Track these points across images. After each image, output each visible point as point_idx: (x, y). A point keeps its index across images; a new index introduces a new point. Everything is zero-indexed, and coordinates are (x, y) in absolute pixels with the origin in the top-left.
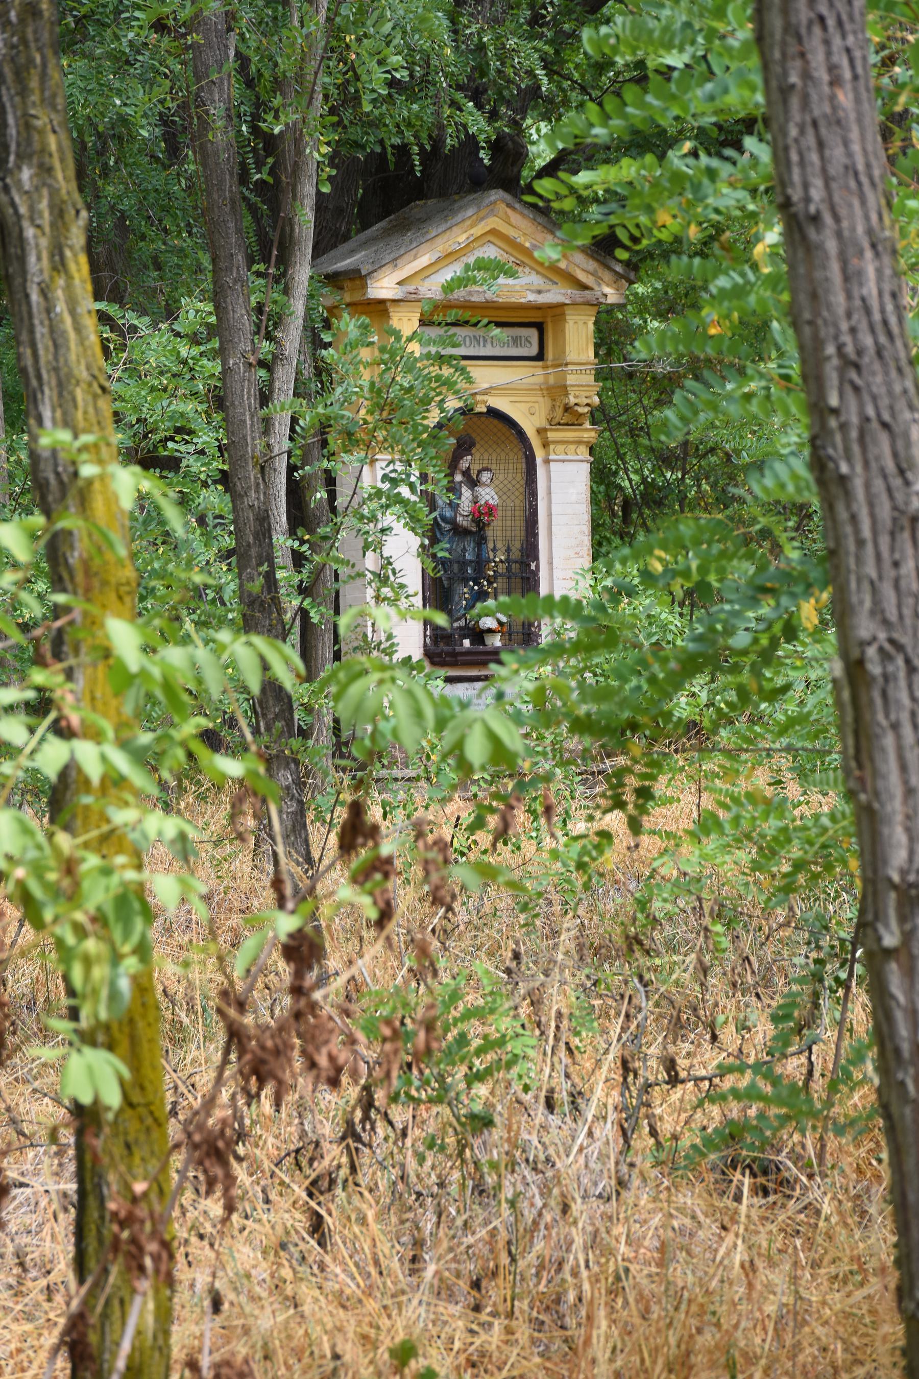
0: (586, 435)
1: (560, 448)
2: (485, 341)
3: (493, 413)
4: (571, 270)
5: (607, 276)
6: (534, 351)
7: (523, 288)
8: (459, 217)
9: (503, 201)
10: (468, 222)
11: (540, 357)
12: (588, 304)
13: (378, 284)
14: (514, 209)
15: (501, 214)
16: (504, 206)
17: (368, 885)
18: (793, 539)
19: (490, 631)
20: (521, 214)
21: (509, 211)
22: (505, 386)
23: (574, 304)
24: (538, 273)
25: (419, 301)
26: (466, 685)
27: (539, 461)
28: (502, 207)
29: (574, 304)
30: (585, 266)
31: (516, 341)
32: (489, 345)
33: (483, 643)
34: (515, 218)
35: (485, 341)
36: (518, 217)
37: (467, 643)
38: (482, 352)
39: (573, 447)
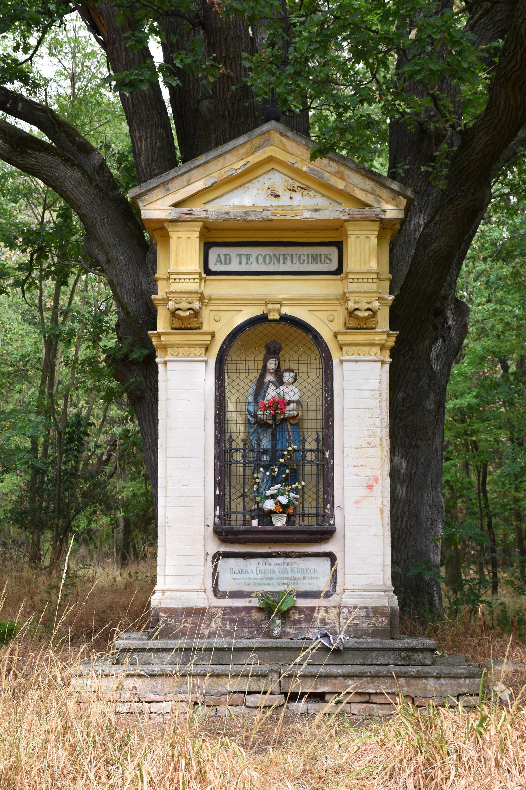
0: (377, 337)
1: (350, 350)
2: (285, 259)
3: (285, 319)
4: (349, 190)
5: (385, 194)
6: (334, 266)
7: (304, 206)
8: (230, 145)
9: (276, 130)
10: (243, 151)
11: (339, 271)
12: (366, 219)
13: (151, 206)
14: (287, 137)
15: (277, 143)
16: (278, 135)
17: (417, 633)
18: (137, 515)
19: (272, 512)
20: (294, 141)
21: (283, 139)
22: (303, 297)
23: (353, 220)
24: (323, 196)
25: (195, 220)
26: (260, 560)
27: (335, 362)
28: (276, 137)
29: (353, 220)
30: (362, 186)
31: (315, 258)
32: (288, 262)
33: (271, 523)
34: (290, 145)
35: (285, 259)
36: (294, 144)
37: (255, 523)
38: (282, 269)
39: (366, 349)
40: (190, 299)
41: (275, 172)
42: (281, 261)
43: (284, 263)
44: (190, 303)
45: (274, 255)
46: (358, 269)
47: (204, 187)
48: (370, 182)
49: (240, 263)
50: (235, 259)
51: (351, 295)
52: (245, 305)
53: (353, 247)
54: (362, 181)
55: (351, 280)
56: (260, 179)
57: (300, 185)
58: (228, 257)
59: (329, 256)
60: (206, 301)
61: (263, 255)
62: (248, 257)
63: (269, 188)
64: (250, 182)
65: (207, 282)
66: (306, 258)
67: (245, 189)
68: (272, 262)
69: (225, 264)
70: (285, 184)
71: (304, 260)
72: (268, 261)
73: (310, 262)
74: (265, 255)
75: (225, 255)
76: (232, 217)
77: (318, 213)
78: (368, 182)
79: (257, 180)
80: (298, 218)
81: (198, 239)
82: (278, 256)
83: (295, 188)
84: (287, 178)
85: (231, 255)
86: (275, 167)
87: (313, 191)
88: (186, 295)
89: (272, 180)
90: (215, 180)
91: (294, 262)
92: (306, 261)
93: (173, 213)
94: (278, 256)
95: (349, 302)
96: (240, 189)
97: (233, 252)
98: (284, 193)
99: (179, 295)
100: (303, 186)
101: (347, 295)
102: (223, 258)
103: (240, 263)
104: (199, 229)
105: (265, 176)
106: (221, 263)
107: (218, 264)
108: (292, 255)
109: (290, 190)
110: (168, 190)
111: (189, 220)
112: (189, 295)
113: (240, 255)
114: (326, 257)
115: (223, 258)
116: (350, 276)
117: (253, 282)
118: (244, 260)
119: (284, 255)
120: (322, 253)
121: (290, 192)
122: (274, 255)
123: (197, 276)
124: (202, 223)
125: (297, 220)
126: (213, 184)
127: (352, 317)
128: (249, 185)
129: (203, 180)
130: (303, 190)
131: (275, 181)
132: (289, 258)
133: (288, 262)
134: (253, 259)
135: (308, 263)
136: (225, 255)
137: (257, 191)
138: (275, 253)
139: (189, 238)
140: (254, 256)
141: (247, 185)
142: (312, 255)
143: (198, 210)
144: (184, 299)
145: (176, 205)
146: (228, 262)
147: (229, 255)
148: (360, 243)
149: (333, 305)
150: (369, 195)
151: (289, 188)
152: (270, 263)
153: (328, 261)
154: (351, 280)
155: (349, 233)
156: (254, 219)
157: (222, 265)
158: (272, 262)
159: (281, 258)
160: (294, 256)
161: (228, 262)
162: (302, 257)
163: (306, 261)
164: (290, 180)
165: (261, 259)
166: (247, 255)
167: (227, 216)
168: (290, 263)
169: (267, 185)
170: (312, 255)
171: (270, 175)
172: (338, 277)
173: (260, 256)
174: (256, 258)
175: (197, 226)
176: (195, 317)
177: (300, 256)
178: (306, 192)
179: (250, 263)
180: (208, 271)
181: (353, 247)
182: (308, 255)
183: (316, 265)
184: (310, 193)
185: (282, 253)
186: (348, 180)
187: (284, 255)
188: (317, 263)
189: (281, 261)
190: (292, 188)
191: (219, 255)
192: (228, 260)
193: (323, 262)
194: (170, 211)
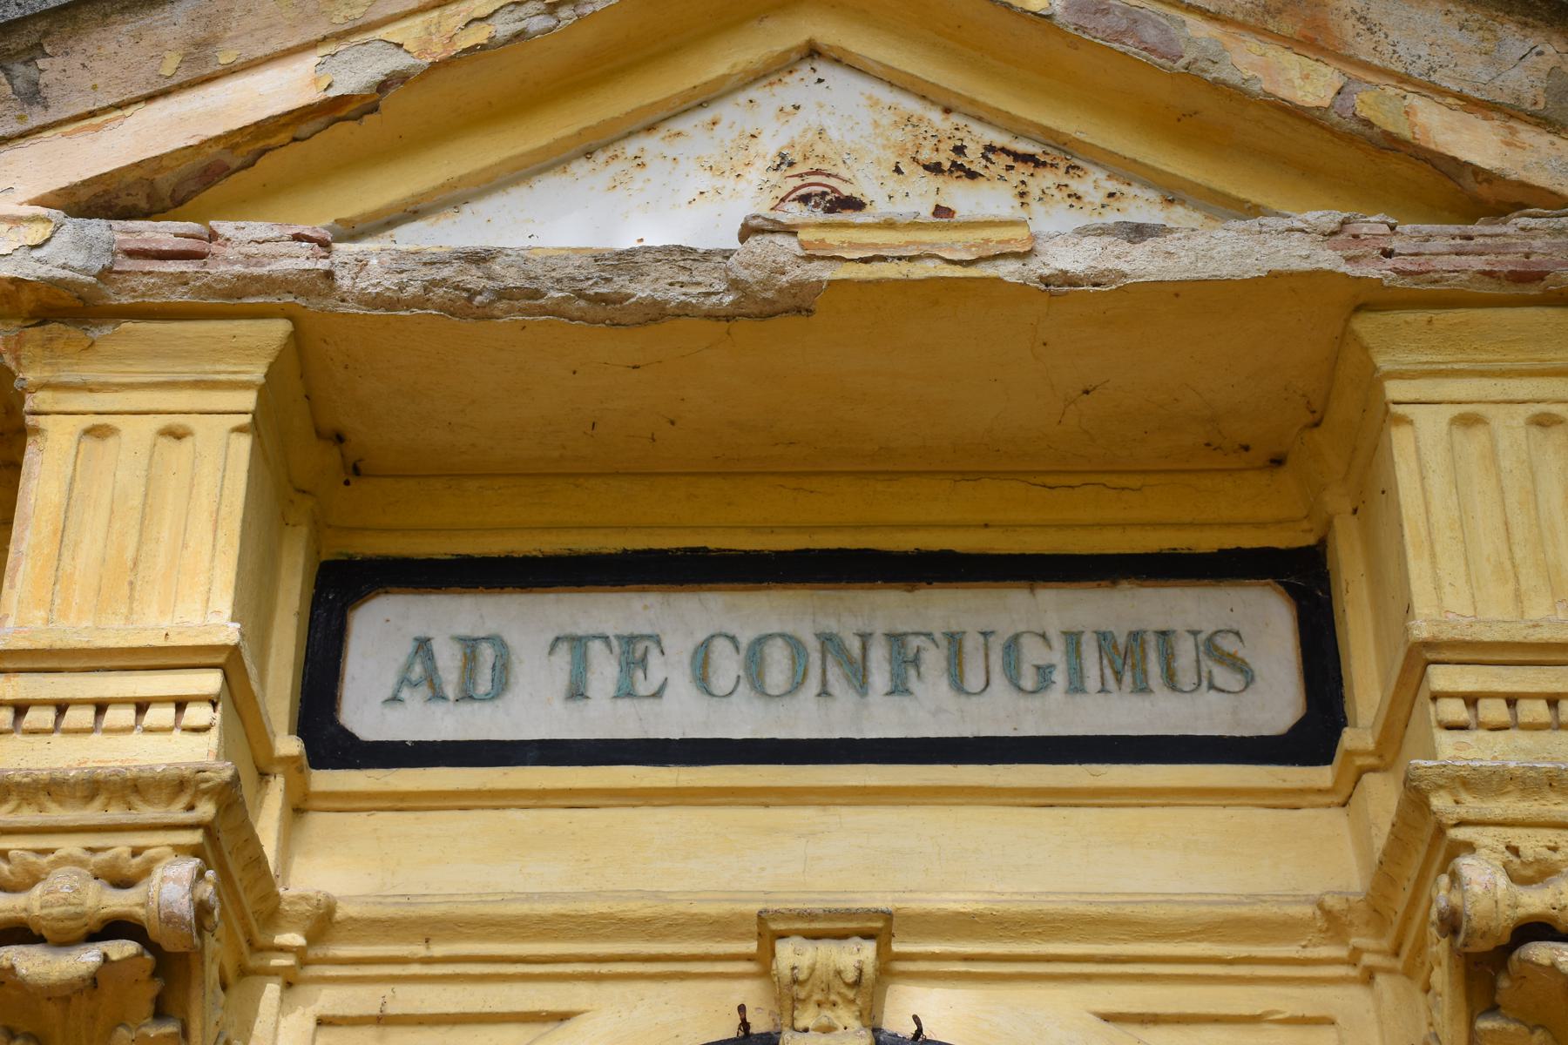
11: (1314, 737)
30: (1473, 73)
31: (1127, 658)
32: (932, 685)
38: (884, 719)
40: (121, 845)
41: (823, 69)
42: (880, 678)
43: (899, 688)
44: (123, 883)
45: (828, 641)
46: (1496, 618)
47: (313, 96)
48: (1536, 39)
49: (577, 692)
50: (542, 665)
51: (1472, 806)
52: (597, 970)
53: (1438, 484)
54: (1469, 40)
55: (1455, 710)
56: (729, 112)
57: (1000, 140)
58: (487, 654)
59: (1228, 644)
60: (294, 938)
61: (745, 639)
62: (634, 652)
63: (784, 162)
64: (650, 129)
65: (319, 822)
66: (1057, 656)
67: (616, 167)
68: (813, 684)
69: (467, 696)
70: (898, 135)
71: (1044, 672)
72: (778, 672)
73: (1092, 682)
74: (761, 641)
75: (470, 646)
76: (512, 279)
77: (1149, 243)
78: (1514, 40)
79: (706, 116)
80: (1007, 271)
81: (244, 443)
82: (854, 646)
83: (973, 158)
84: (911, 105)
85: (513, 638)
86: (827, 32)
87: (1098, 175)
88: (93, 814)
89: (811, 116)
90: (398, 62)
91: (974, 680)
92: (1060, 677)
93: (72, 251)
94: (854, 646)
95: (1468, 866)
96: (581, 168)
97: (525, 622)
98: (893, 183)
99: (28, 816)
100: (1023, 147)
101: (1440, 802)
102: (448, 660)
103: (577, 692)
104: (257, 373)
105: (755, 93)
106: (437, 695)
107: (414, 700)
108: (955, 641)
109: (935, 169)
110: (33, 95)
111: (179, 297)
112: (117, 814)
113: (578, 643)
114: (1211, 648)
115: (448, 660)
116: (1441, 678)
117: (663, 814)
118: (604, 670)
119: (896, 639)
120: (1177, 624)
121: (939, 181)
122: (828, 641)
123: (211, 682)
124: (279, 329)
125: (998, 280)
126: (382, 87)
127: (1493, 1009)
128: (650, 144)
129: (313, 59)
130: (1022, 170)
131: (829, 123)
132: (934, 659)
133: (932, 685)
134: (669, 666)
135: (1076, 686)
136: (470, 646)
137: (705, 181)
138: (831, 625)
139: (177, 434)
140: (680, 647)
141: (631, 147)
142: (1103, 638)
143: (256, 241)
144: (70, 846)
145: (94, 200)
146: (484, 685)
147: (496, 640)
148: (1493, 456)
149: (1298, 972)
150: (1527, 134)
151: (927, 155)
152: (796, 686)
153: (1222, 676)
154: (1455, 710)
155: (1395, 390)
156: (676, 295)
157: (439, 708)
158: (813, 684)
159: (879, 656)
160: (972, 644)
161: (484, 685)
162: (1033, 653)
163: (1060, 677)
164: (935, 116)
165: (726, 667)
166: (631, 640)
167: (473, 277)
168: (943, 685)
169: (769, 147)
170: (1103, 638)
171: (798, 87)
172: (1321, 776)
173: (721, 648)
174: (690, 661)
175: (247, 353)
176: (160, 1014)
177: (1012, 646)
178: (1047, 179)
179: (642, 688)
180: (329, 743)
181: (1438, 484)
182: (1073, 640)
183: (1140, 703)
184: (1075, 185)
185: (880, 627)
186: (1363, 49)
187: (896, 639)
188: (1142, 688)
189: (880, 678)
190: (945, 158)
191: (423, 646)
192: (487, 670)
193: (1186, 678)
194: (37, 233)
